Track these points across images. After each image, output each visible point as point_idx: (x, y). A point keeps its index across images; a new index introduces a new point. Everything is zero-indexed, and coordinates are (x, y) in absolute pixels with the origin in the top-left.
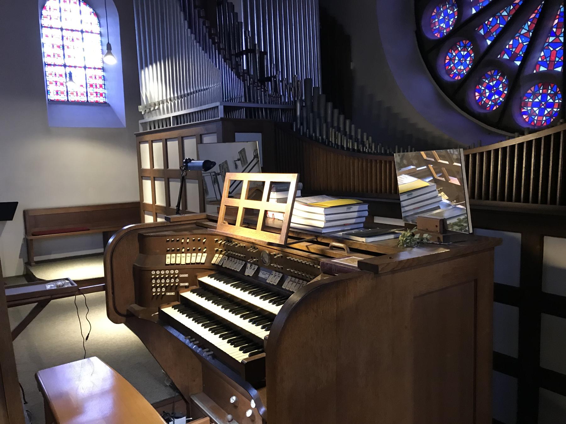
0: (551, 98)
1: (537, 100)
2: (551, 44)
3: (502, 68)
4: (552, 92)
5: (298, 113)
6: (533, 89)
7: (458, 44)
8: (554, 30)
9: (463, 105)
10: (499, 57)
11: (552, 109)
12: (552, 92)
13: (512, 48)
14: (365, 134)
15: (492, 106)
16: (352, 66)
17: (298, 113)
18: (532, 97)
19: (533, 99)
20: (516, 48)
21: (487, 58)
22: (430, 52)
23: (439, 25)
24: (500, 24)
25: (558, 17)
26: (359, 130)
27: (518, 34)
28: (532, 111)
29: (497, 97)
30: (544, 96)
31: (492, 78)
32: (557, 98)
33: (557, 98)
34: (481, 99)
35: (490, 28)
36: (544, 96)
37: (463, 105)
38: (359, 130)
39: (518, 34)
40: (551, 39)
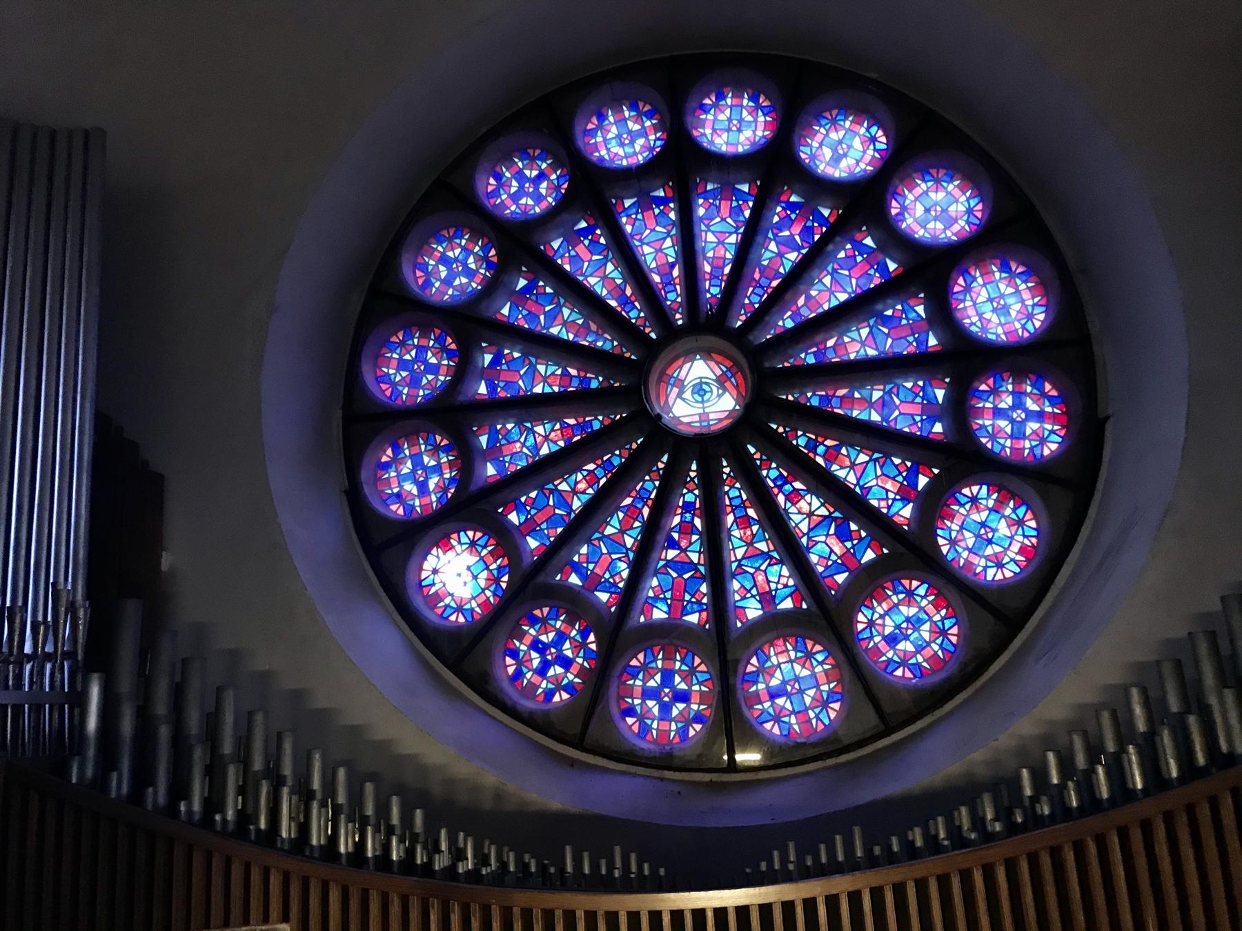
0: (683, 679)
1: (652, 683)
2: (669, 564)
3: (574, 605)
4: (684, 668)
5: (92, 723)
6: (641, 656)
7: (454, 536)
8: (676, 536)
9: (483, 685)
10: (558, 578)
11: (688, 706)
12: (684, 668)
13: (588, 562)
14: (586, 856)
15: (549, 694)
16: (166, 561)
17: (92, 723)
18: (641, 676)
19: (645, 681)
20: (596, 563)
21: (541, 578)
22: (388, 549)
23: (400, 486)
24: (555, 507)
25: (679, 511)
26: (633, 857)
27: (597, 535)
28: (645, 709)
29: (652, 683)
30: (668, 676)
31: (544, 623)
32: (695, 681)
33: (695, 681)
34: (519, 674)
35: (533, 511)
36: (668, 676)
37: (483, 685)
38: (633, 857)
39: (597, 535)
40: (671, 554)
